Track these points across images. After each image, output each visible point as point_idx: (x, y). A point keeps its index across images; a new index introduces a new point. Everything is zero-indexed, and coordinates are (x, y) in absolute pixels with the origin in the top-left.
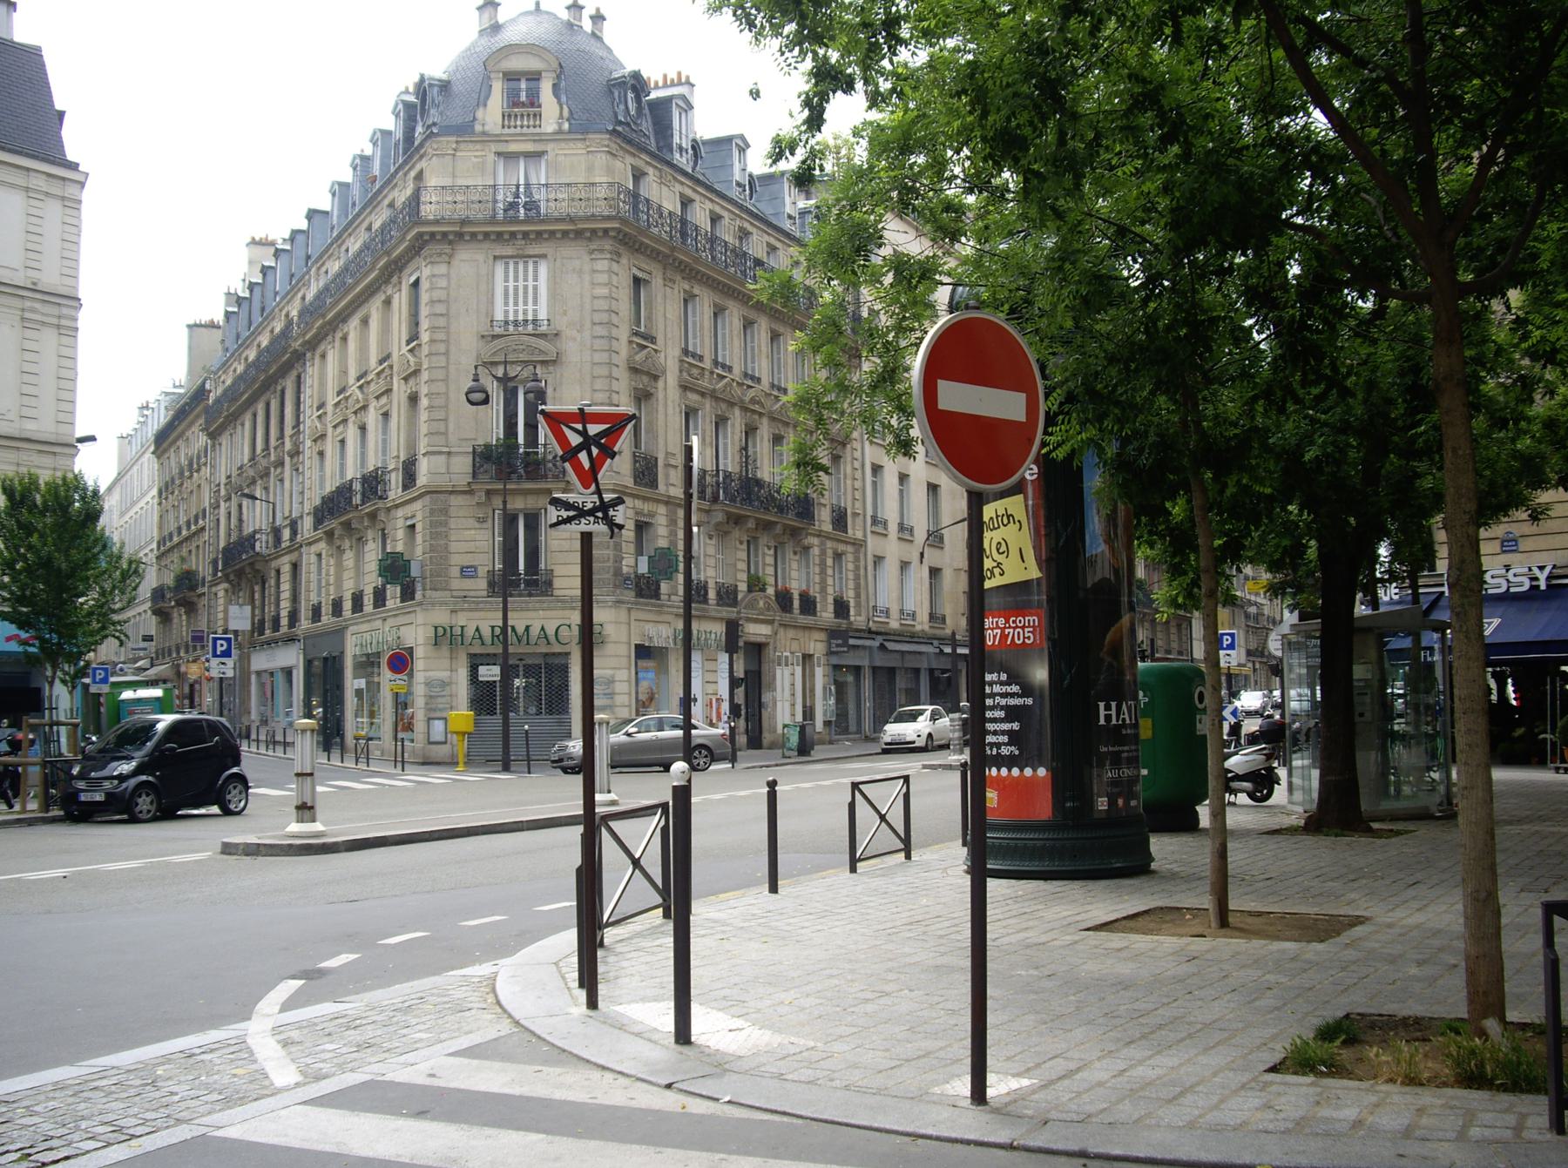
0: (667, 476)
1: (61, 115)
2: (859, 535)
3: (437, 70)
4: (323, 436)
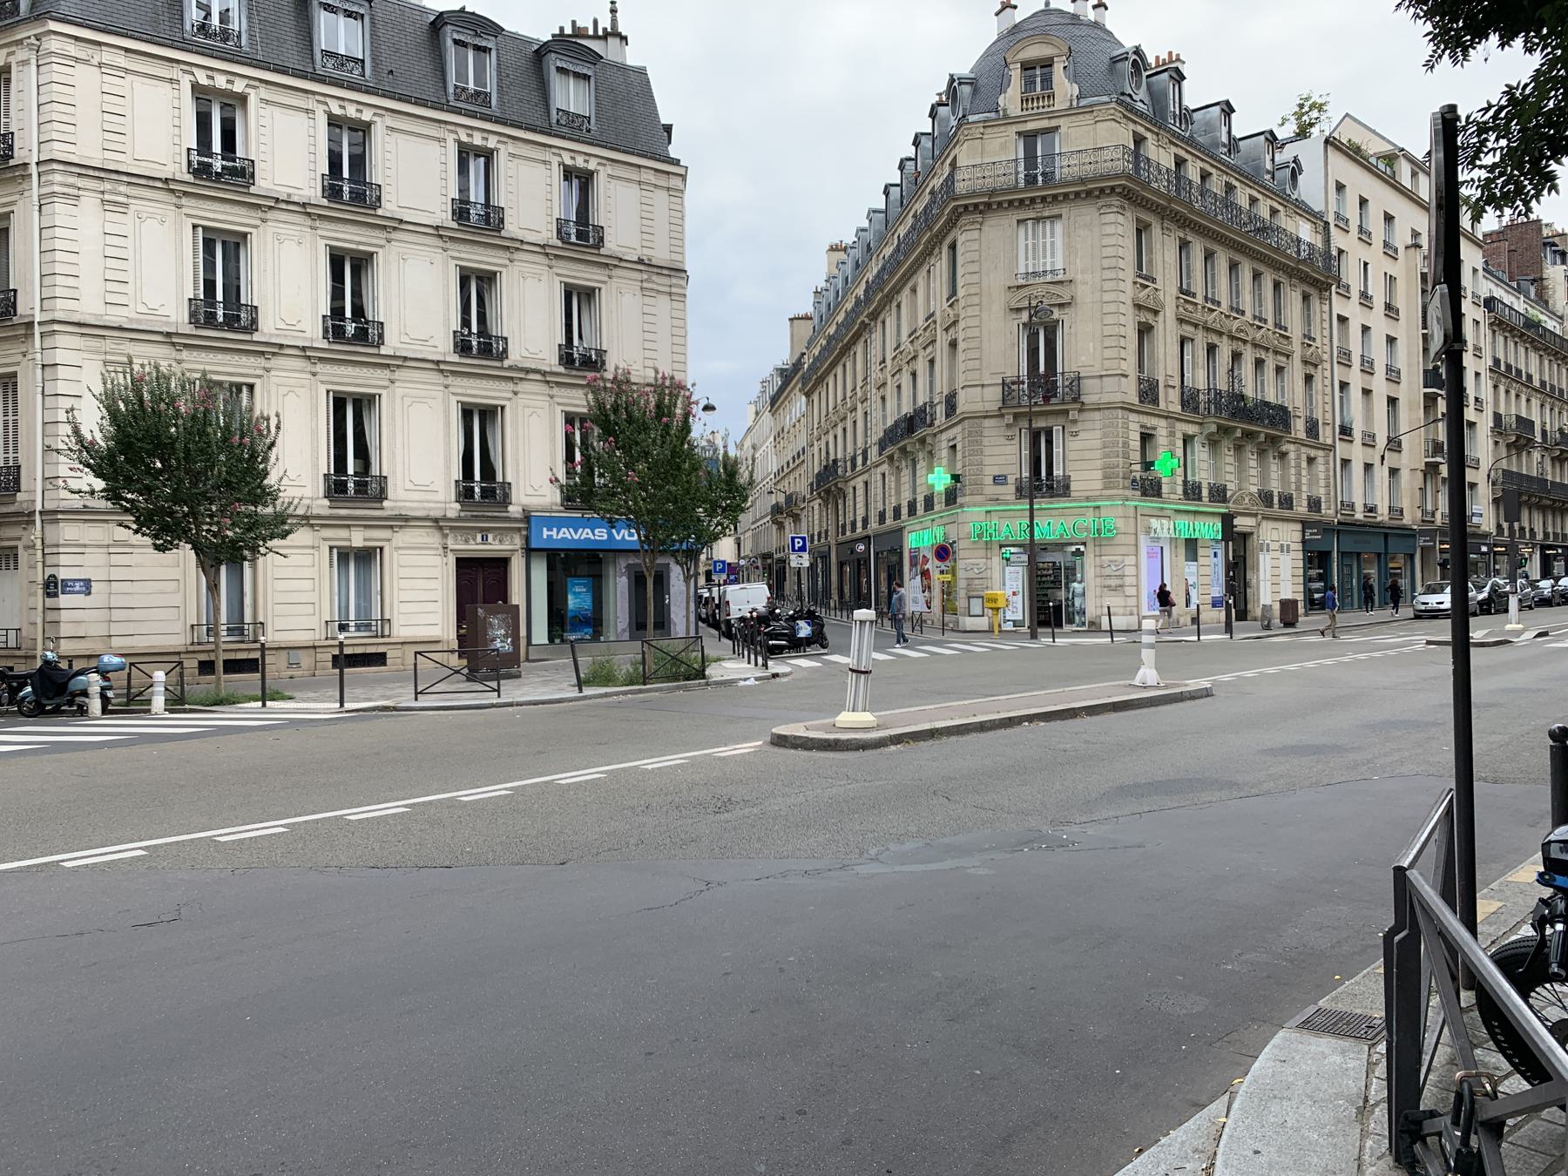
0: (1166, 394)
1: (668, 129)
2: (1329, 441)
3: (964, 69)
4: (884, 384)
